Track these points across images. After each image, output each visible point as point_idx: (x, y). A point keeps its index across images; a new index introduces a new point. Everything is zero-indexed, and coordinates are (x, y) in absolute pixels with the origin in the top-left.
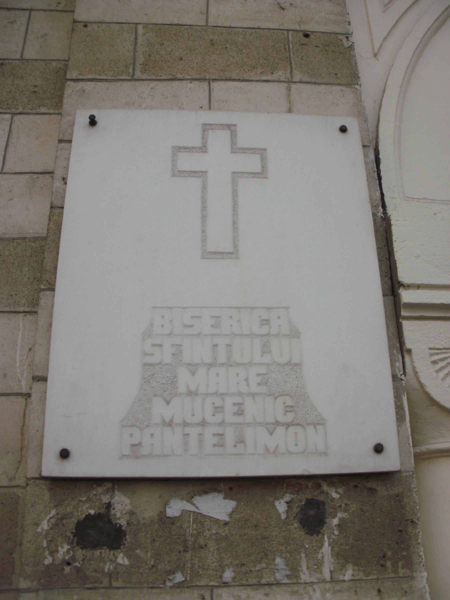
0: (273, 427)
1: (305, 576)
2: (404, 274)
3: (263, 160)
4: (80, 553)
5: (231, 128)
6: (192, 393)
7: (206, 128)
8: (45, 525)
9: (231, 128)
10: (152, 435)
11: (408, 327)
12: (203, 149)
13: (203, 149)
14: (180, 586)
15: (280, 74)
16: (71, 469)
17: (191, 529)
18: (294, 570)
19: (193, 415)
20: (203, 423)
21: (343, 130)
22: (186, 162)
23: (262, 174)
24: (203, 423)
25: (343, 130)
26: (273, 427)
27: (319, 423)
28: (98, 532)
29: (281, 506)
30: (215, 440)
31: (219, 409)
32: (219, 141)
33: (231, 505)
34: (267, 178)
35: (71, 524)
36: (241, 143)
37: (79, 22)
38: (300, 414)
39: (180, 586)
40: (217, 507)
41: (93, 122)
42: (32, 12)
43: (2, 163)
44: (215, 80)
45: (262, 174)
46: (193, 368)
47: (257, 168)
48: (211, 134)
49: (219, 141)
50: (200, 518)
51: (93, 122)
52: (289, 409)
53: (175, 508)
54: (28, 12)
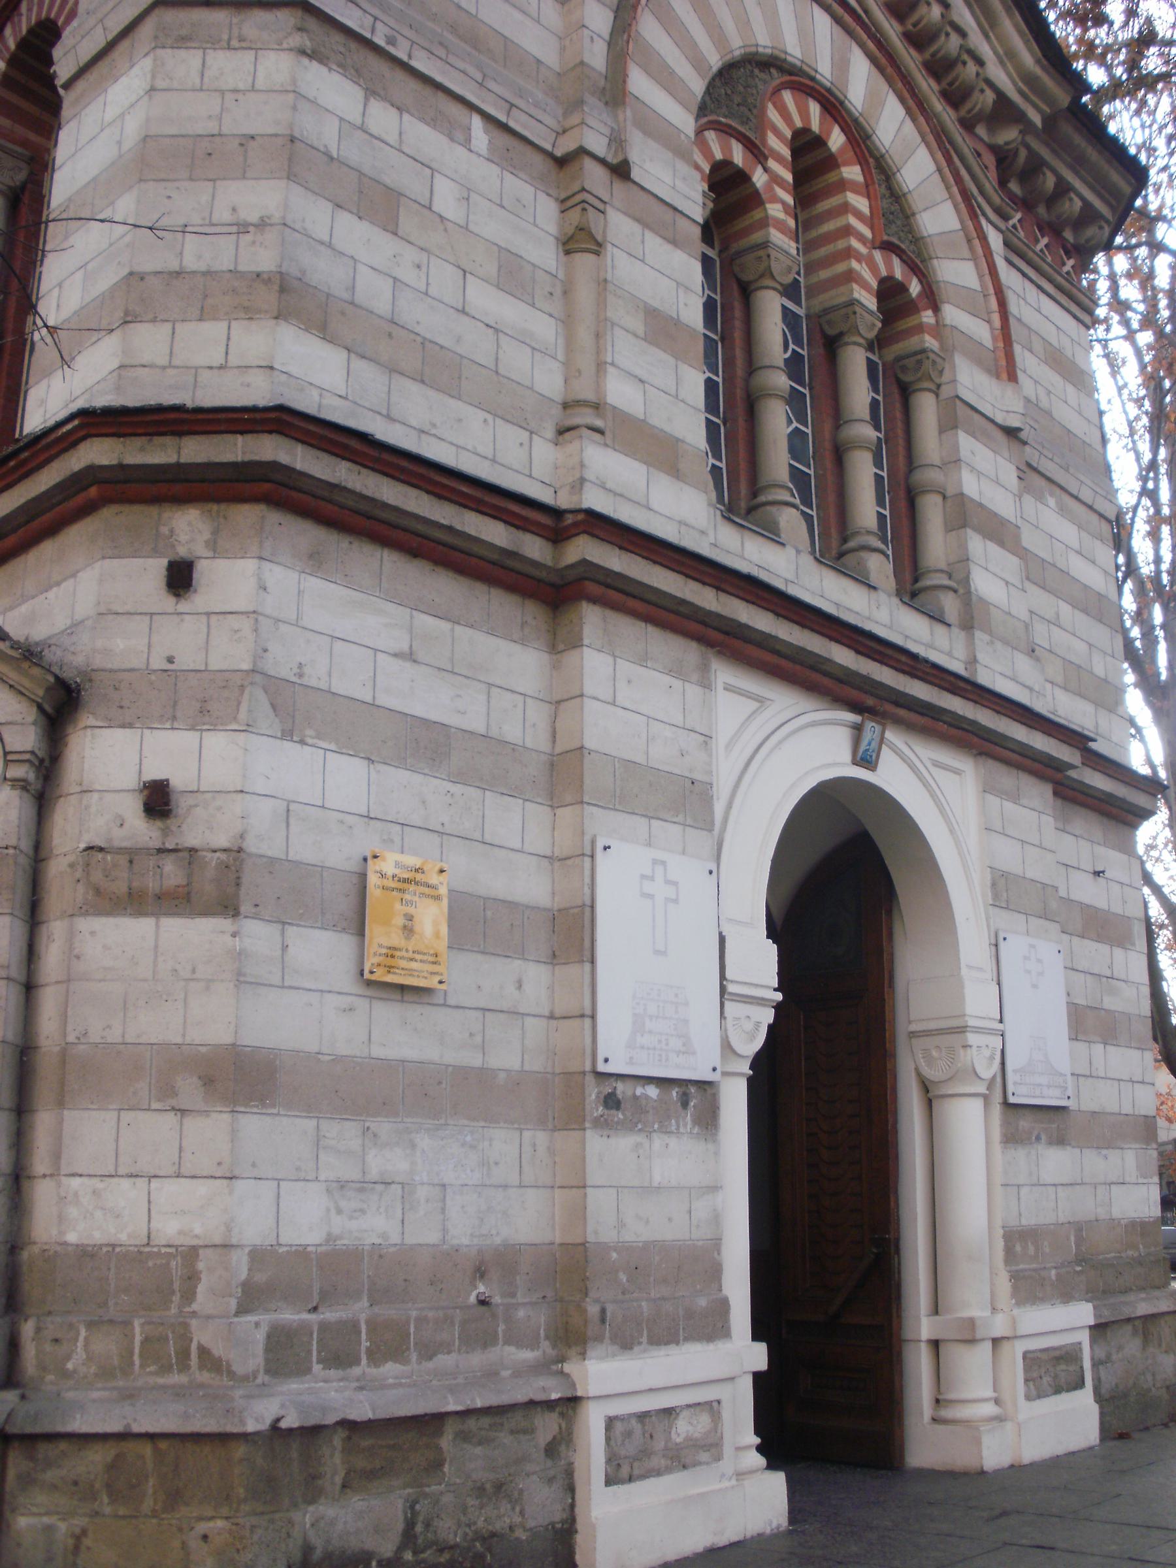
0: (678, 1053)
1: (682, 1130)
2: (728, 975)
4: (606, 1112)
6: (650, 1032)
8: (593, 1097)
11: (727, 1004)
14: (640, 1130)
15: (680, 818)
16: (609, 1068)
17: (644, 1102)
18: (678, 1128)
20: (654, 1049)
24: (654, 1049)
26: (678, 1053)
27: (694, 1053)
28: (611, 1101)
29: (674, 1094)
31: (660, 1041)
33: (657, 1091)
35: (602, 1097)
38: (688, 1050)
39: (640, 1130)
40: (652, 1091)
42: (154, 617)
46: (651, 1017)
50: (647, 1097)
52: (684, 1045)
53: (639, 1091)
54: (148, 617)
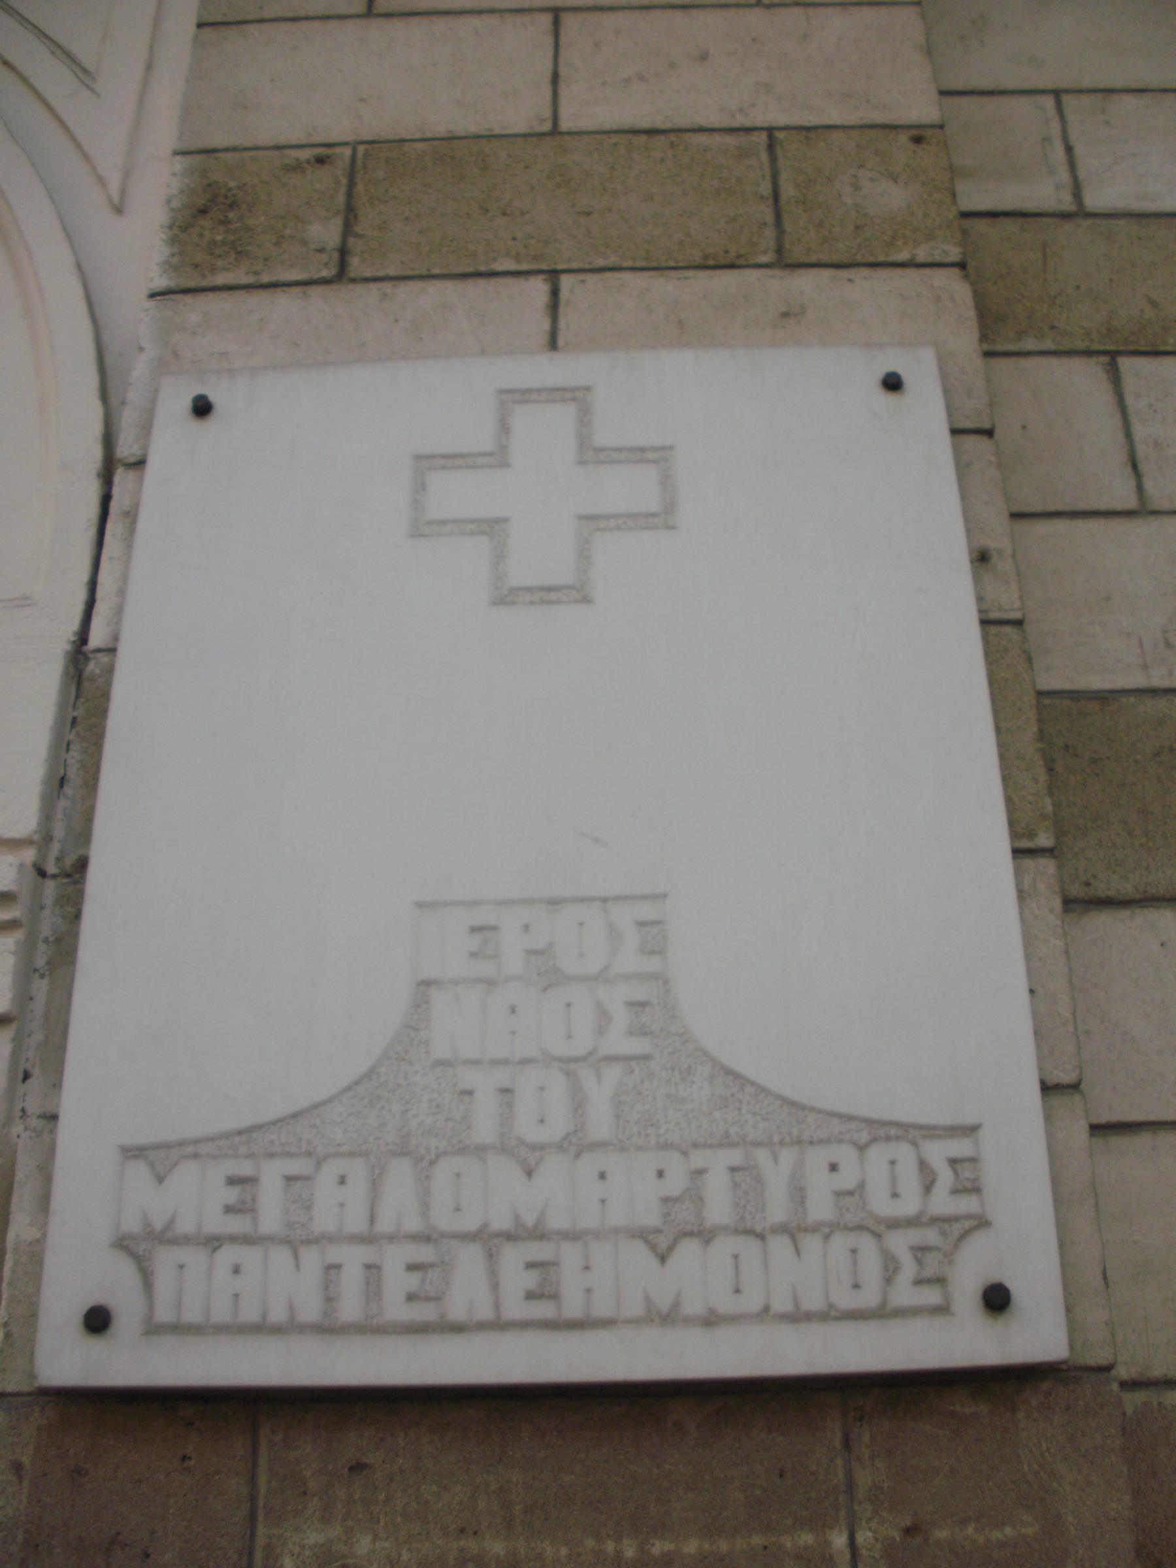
3: (667, 482)
5: (577, 397)
7: (513, 398)
9: (577, 397)
10: (342, 1180)
12: (499, 458)
13: (499, 458)
16: (129, 1363)
19: (458, 1175)
21: (892, 383)
22: (454, 495)
23: (663, 518)
25: (892, 383)
30: (530, 1280)
32: (545, 434)
34: (672, 528)
36: (605, 436)
37: (329, 1101)
41: (202, 408)
43: (506, 5)
44: (1064, 216)
45: (663, 518)
47: (650, 501)
48: (524, 419)
49: (545, 434)
51: (202, 408)
